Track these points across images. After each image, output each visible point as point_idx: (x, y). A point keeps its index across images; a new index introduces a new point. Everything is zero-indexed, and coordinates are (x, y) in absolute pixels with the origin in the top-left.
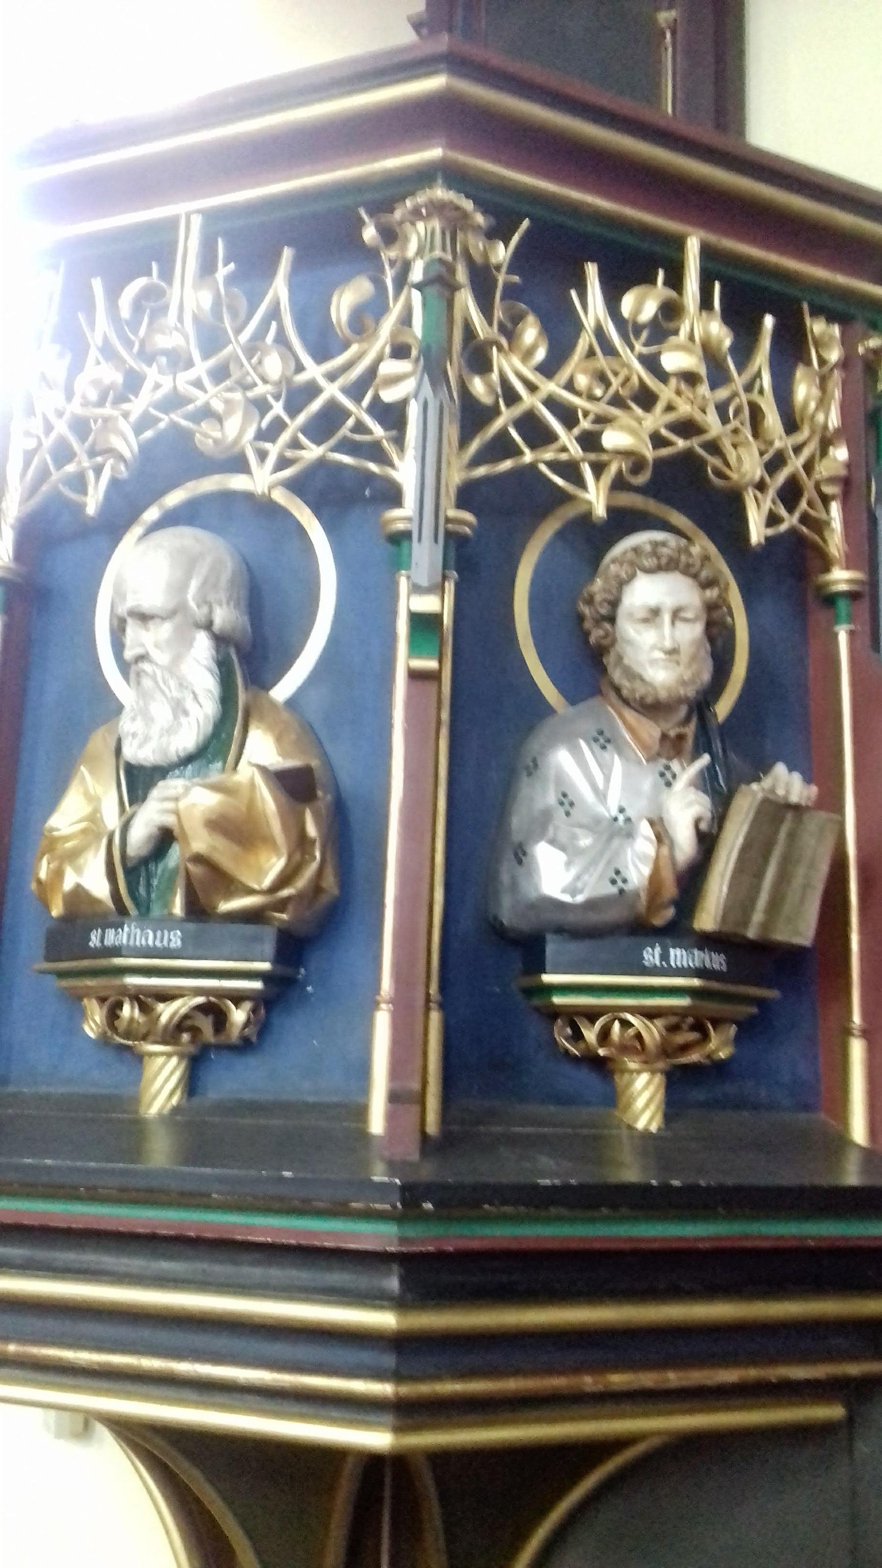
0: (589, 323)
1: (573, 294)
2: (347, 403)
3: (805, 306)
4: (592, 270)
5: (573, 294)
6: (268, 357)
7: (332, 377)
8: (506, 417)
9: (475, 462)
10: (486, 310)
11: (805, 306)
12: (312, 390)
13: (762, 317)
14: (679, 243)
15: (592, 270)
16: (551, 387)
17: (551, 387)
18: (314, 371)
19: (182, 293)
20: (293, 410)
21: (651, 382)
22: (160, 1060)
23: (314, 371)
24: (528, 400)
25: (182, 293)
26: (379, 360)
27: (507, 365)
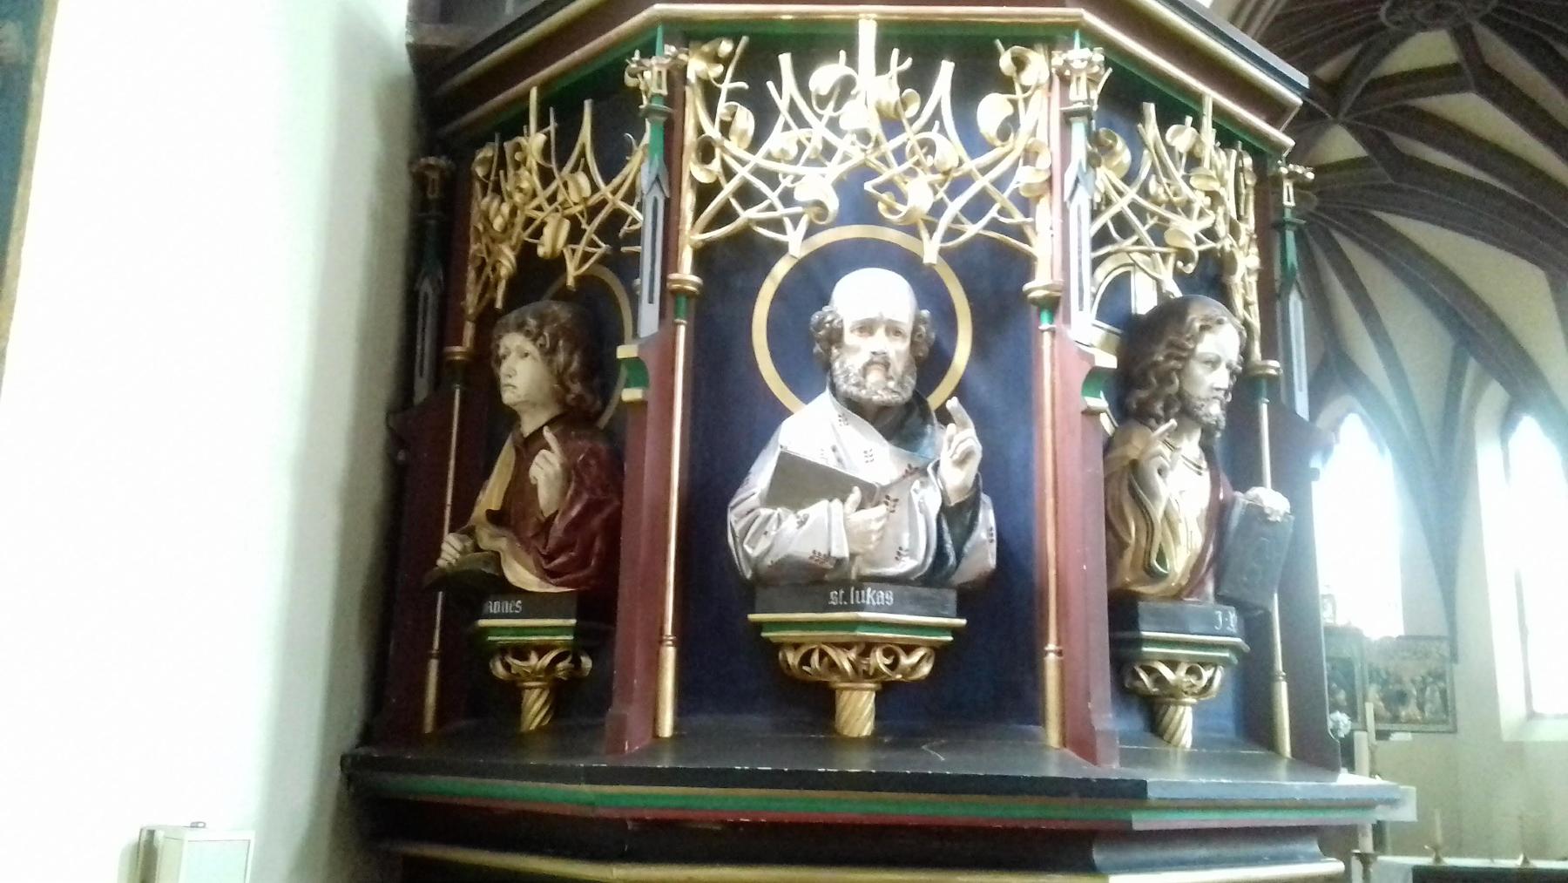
0: (783, 104)
1: (770, 85)
2: (624, 206)
3: (998, 43)
4: (1150, 109)
5: (770, 85)
6: (1366, 633)
7: (984, 171)
8: (729, 188)
9: (710, 227)
10: (712, 111)
11: (998, 43)
12: (967, 180)
13: (624, 139)
14: (851, 26)
15: (1150, 109)
16: (758, 159)
17: (758, 159)
18: (971, 165)
19: (1525, 658)
20: (954, 192)
21: (832, 138)
22: (537, 692)
23: (605, 190)
24: (743, 173)
25: (1525, 658)
26: (1015, 167)
27: (735, 146)
